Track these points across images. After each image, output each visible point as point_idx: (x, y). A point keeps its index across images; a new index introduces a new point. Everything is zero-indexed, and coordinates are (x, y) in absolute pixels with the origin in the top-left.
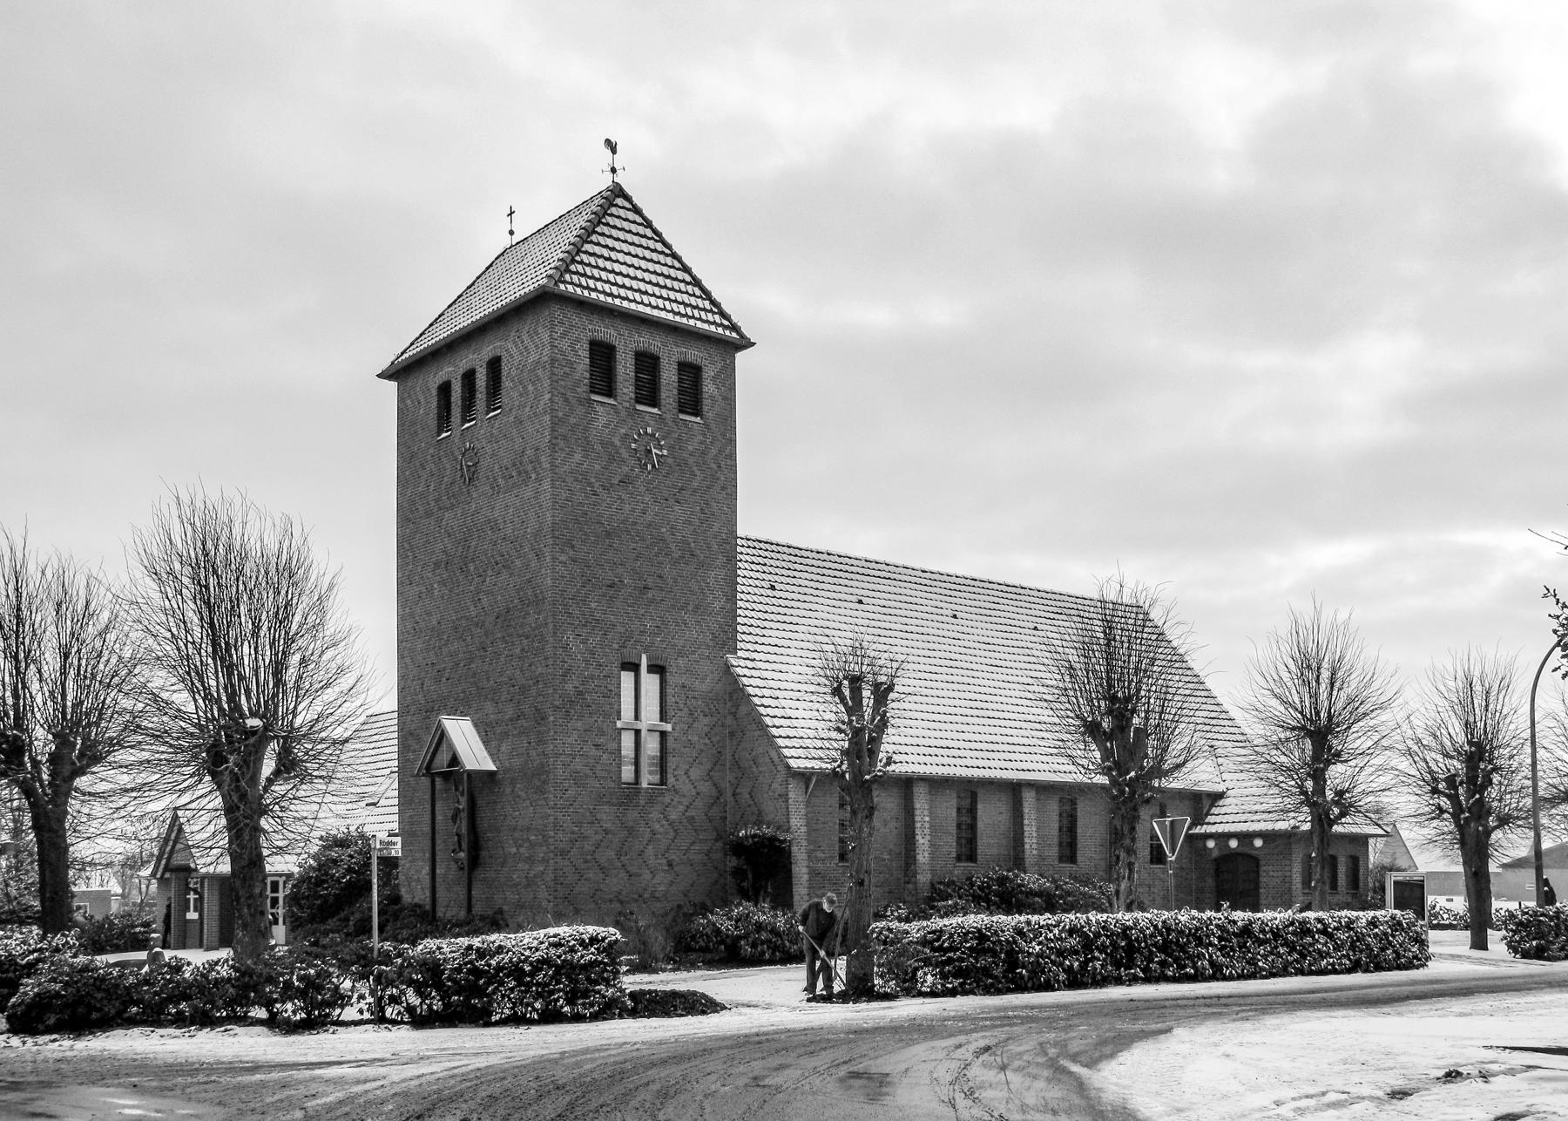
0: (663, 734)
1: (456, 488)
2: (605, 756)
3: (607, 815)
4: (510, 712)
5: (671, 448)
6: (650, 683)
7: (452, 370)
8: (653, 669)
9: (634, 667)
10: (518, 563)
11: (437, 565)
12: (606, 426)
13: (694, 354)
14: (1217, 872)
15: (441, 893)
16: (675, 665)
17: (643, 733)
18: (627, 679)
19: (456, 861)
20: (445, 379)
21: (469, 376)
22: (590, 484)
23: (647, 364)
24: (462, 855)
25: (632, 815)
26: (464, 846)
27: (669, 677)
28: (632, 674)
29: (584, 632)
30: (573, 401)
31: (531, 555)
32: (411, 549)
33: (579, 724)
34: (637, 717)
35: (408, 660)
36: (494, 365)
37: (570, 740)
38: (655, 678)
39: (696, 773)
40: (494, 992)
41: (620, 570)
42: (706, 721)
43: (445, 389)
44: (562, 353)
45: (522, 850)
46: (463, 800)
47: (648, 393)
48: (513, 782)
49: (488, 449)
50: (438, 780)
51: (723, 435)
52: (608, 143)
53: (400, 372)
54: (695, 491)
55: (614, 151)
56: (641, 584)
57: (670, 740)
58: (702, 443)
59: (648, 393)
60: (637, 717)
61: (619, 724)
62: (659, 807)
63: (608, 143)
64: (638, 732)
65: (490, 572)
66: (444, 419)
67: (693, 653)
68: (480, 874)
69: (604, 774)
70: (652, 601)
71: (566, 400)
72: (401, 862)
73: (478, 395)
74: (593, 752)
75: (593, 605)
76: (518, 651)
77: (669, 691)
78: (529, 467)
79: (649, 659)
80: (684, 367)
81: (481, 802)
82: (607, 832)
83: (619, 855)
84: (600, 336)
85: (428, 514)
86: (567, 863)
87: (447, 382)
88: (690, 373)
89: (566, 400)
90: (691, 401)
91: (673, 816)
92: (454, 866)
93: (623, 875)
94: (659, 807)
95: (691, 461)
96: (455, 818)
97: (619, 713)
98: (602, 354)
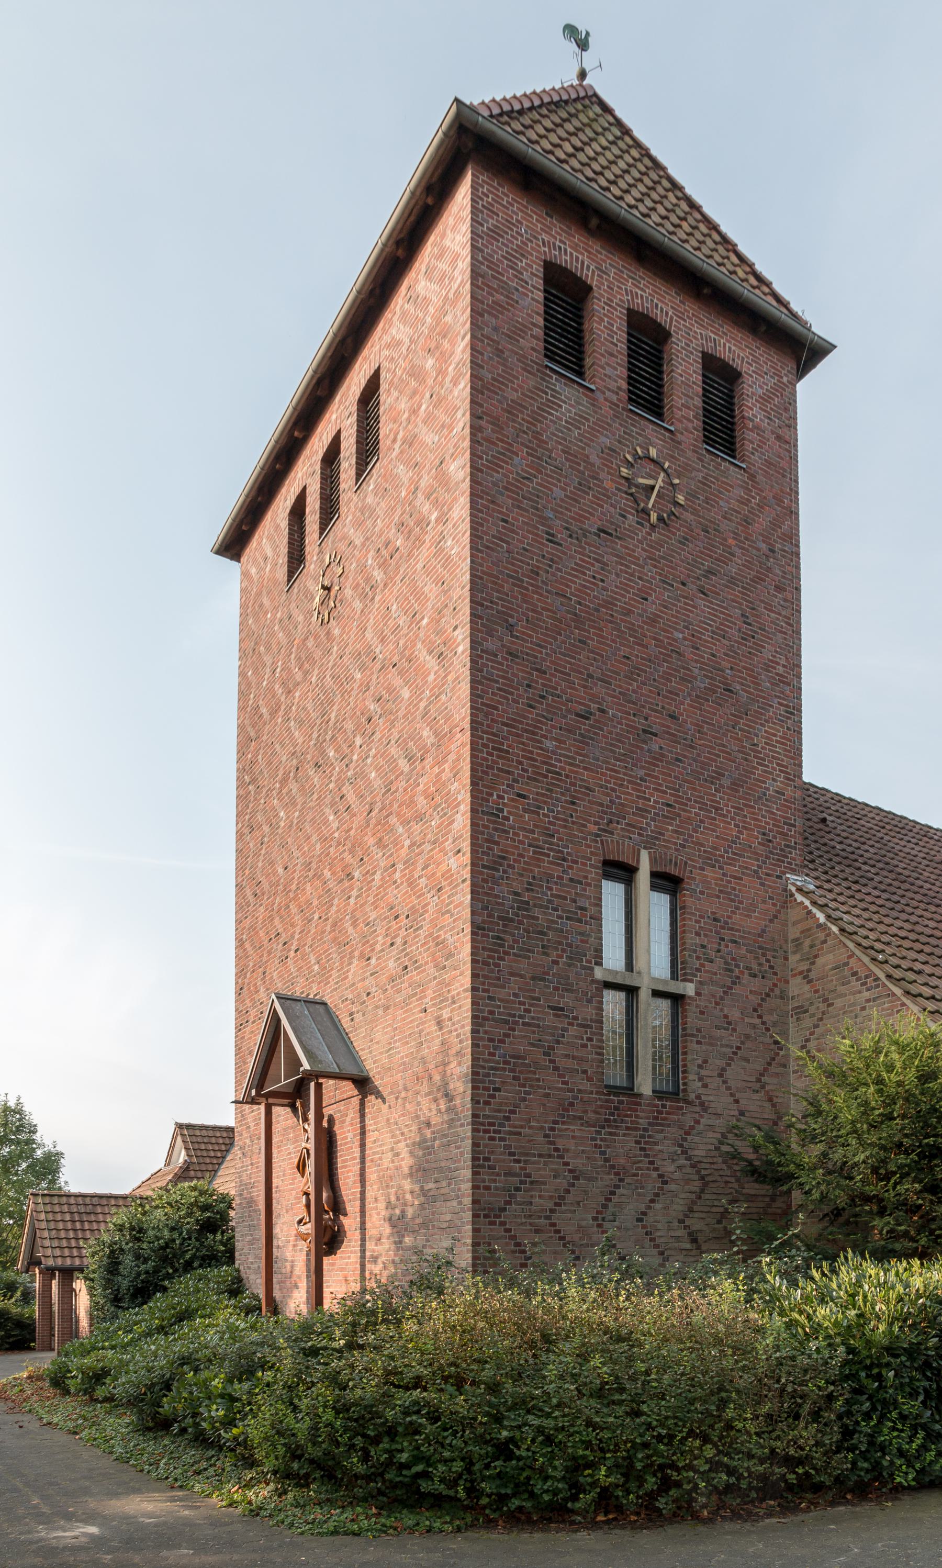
0: (677, 999)
2: (573, 1031)
3: (576, 1140)
6: (656, 909)
8: (666, 881)
9: (622, 871)
12: (574, 423)
13: (734, 347)
15: (352, 1114)
16: (702, 879)
17: (644, 995)
18: (612, 894)
22: (543, 520)
23: (647, 341)
25: (624, 1145)
27: (687, 897)
30: (512, 360)
33: (523, 966)
37: (502, 993)
39: (737, 1074)
41: (599, 689)
42: (756, 984)
47: (647, 391)
51: (779, 501)
52: (570, 30)
54: (732, 581)
55: (583, 45)
56: (640, 723)
57: (692, 1019)
58: (741, 502)
59: (647, 391)
61: (599, 974)
62: (674, 1132)
63: (570, 30)
64: (632, 991)
69: (571, 1064)
70: (658, 758)
71: (499, 352)
72: (594, 874)
74: (549, 1019)
75: (549, 744)
79: (653, 861)
82: (576, 1175)
83: (600, 1221)
84: (564, 260)
88: (720, 377)
89: (499, 352)
90: (721, 428)
91: (699, 1153)
94: (674, 1132)
95: (725, 526)
98: (566, 295)
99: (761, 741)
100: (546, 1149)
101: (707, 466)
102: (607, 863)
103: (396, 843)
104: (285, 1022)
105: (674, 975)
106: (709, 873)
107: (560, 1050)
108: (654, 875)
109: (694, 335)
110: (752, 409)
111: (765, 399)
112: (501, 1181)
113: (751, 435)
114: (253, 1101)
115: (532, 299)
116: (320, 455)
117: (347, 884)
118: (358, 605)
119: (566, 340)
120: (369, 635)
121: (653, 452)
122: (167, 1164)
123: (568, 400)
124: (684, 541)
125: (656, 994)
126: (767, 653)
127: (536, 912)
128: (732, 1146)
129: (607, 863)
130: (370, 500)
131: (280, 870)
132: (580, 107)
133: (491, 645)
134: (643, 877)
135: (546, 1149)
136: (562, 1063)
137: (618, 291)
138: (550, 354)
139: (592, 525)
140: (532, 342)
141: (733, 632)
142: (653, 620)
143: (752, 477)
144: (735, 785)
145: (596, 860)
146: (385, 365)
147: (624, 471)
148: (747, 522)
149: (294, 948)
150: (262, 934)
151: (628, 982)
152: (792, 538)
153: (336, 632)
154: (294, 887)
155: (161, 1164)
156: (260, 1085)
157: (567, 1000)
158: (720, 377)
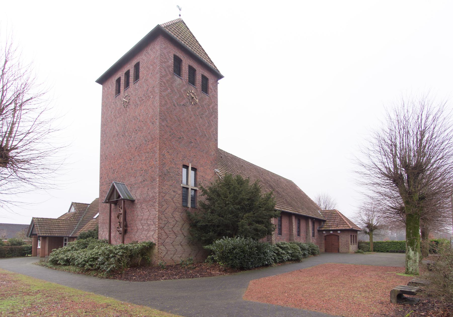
0: (195, 190)
1: (122, 110)
4: (140, 179)
6: (192, 173)
7: (121, 74)
8: (193, 169)
9: (186, 167)
10: (145, 128)
11: (114, 136)
12: (179, 85)
13: (207, 74)
14: (325, 239)
16: (200, 169)
17: (190, 189)
18: (184, 170)
19: (119, 231)
20: (118, 77)
21: (127, 74)
22: (173, 102)
23: (192, 71)
24: (121, 229)
26: (122, 225)
28: (186, 170)
29: (170, 151)
31: (150, 124)
32: (105, 134)
34: (187, 184)
35: (103, 168)
36: (137, 66)
37: (164, 188)
38: (193, 172)
40: (133, 276)
43: (119, 81)
44: (164, 54)
45: (145, 227)
46: (122, 211)
47: (192, 81)
48: (141, 204)
49: (134, 94)
50: (113, 205)
51: (215, 102)
52: (178, 7)
53: (102, 80)
55: (180, 10)
59: (192, 81)
60: (187, 184)
61: (182, 185)
63: (178, 7)
65: (133, 134)
66: (118, 91)
67: (205, 166)
68: (127, 236)
72: (181, 167)
73: (131, 77)
74: (173, 193)
75: (174, 143)
76: (144, 158)
77: (198, 177)
78: (150, 94)
79: (192, 165)
80: (203, 77)
81: (128, 211)
82: (177, 221)
85: (112, 121)
86: (163, 231)
87: (119, 77)
88: (205, 79)
90: (205, 88)
92: (118, 233)
93: (172, 242)
96: (118, 217)
97: (182, 181)
98: (178, 61)
99: (211, 145)
100: (172, 217)
101: (203, 95)
102: (183, 165)
103: (142, 156)
104: (116, 187)
105: (195, 186)
106: (201, 168)
107: (175, 199)
108: (192, 168)
109: (200, 72)
110: (210, 86)
111: (212, 84)
112: (163, 222)
113: (210, 90)
114: (107, 203)
115: (171, 62)
117: (130, 161)
118: (133, 107)
119: (178, 70)
120: (136, 114)
122: (69, 211)
123: (178, 80)
124: (198, 108)
125: (192, 189)
126: (212, 129)
127: (171, 173)
129: (183, 165)
130: (137, 87)
131: (113, 155)
132: (180, 25)
134: (190, 168)
135: (172, 217)
136: (175, 201)
137: (186, 62)
138: (174, 71)
139: (182, 103)
140: (171, 69)
141: (206, 125)
142: (192, 122)
143: (210, 98)
144: (206, 153)
145: (182, 165)
146: (141, 62)
147: (188, 94)
148: (209, 106)
149: (117, 171)
150: (107, 167)
151: (187, 187)
152: (217, 109)
153: (128, 110)
154: (116, 159)
155: (67, 211)
156: (109, 199)
157: (176, 190)
158: (205, 79)
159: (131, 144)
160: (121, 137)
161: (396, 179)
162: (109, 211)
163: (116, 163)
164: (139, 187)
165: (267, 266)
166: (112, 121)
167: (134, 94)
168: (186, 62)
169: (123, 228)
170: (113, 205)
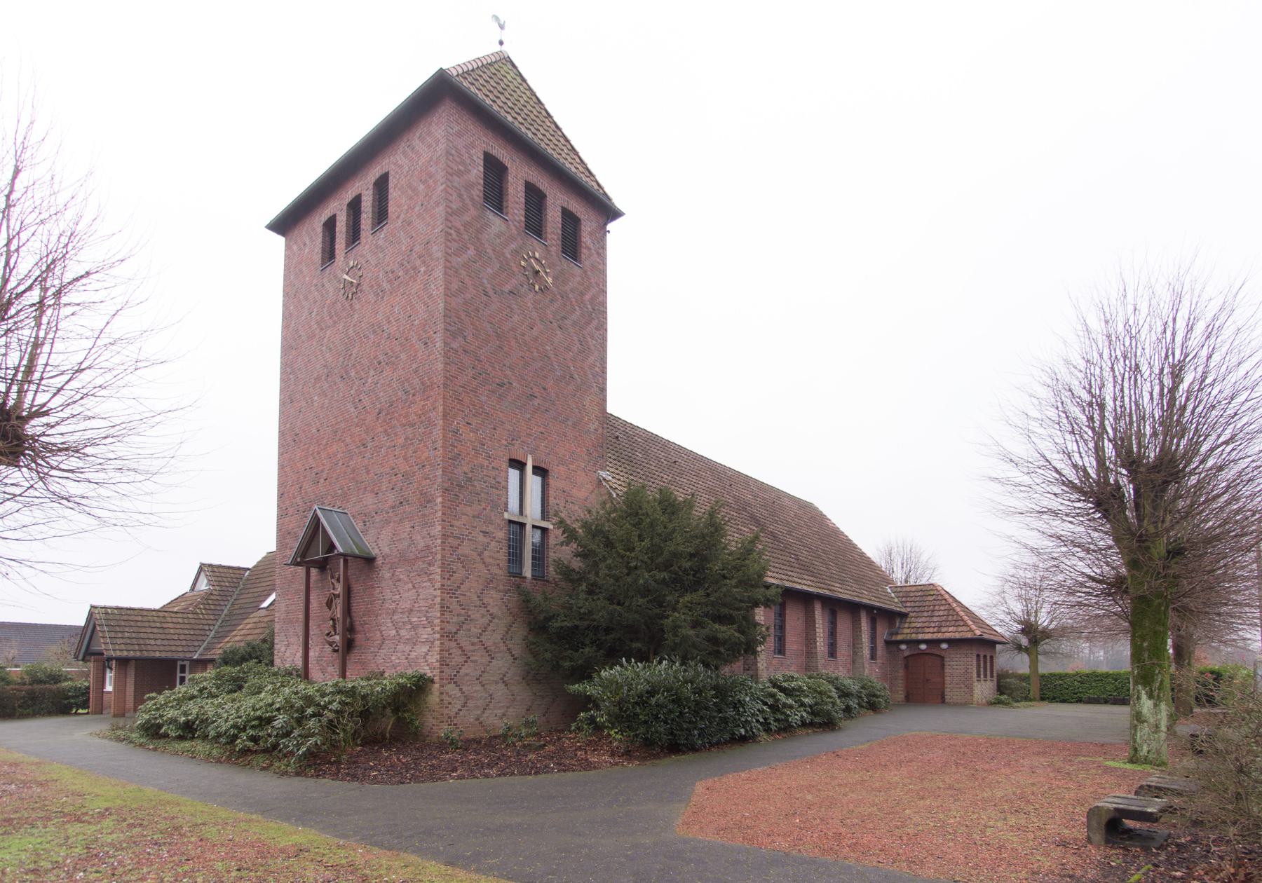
0: (544, 531)
1: (339, 306)
4: (391, 498)
5: (555, 278)
6: (534, 482)
7: (337, 207)
8: (538, 470)
9: (519, 465)
10: (403, 356)
11: (318, 379)
12: (498, 236)
13: (576, 207)
14: (906, 667)
16: (556, 472)
17: (529, 528)
18: (514, 474)
19: (331, 644)
20: (330, 215)
22: (482, 284)
23: (535, 198)
24: (337, 638)
26: (339, 628)
28: (517, 472)
29: (474, 421)
31: (419, 345)
32: (293, 372)
34: (521, 512)
35: (287, 469)
36: (382, 185)
37: (457, 523)
38: (538, 479)
43: (330, 225)
44: (457, 150)
45: (403, 632)
46: (339, 589)
47: (534, 225)
48: (393, 567)
49: (373, 261)
50: (314, 571)
51: (598, 285)
52: (496, 18)
53: (285, 224)
55: (502, 27)
59: (534, 225)
60: (521, 512)
61: (506, 516)
63: (496, 18)
65: (372, 373)
66: (329, 254)
67: (572, 463)
68: (353, 657)
72: (505, 465)
73: (364, 216)
74: (481, 538)
75: (483, 398)
76: (401, 441)
77: (552, 492)
78: (418, 262)
79: (534, 460)
80: (566, 213)
81: (357, 588)
82: (493, 616)
85: (311, 337)
86: (453, 644)
87: (332, 213)
88: (571, 221)
90: (571, 246)
92: (328, 649)
93: (479, 673)
96: (329, 604)
97: (506, 504)
98: (495, 171)
99: (587, 403)
100: (478, 603)
101: (566, 264)
102: (511, 460)
104: (323, 520)
105: (543, 518)
106: (561, 467)
107: (486, 554)
108: (534, 467)
109: (557, 200)
110: (586, 239)
111: (591, 234)
112: (455, 619)
113: (584, 251)
114: (298, 564)
115: (477, 172)
116: (347, 201)
117: (362, 449)
118: (372, 297)
119: (495, 195)
120: (380, 316)
121: (537, 255)
122: (193, 589)
123: (496, 223)
124: (552, 301)
125: (534, 527)
126: (591, 360)
127: (476, 483)
128: (12, 317)
129: (511, 460)
131: (314, 431)
132: (500, 68)
133: (455, 345)
134: (529, 468)
135: (478, 603)
136: (487, 560)
137: (519, 174)
138: (486, 198)
139: (507, 288)
140: (478, 192)
142: (536, 339)
143: (585, 272)
144: (575, 425)
145: (506, 459)
146: (392, 173)
148: (582, 294)
149: (325, 476)
151: (521, 520)
152: (604, 304)
154: (324, 442)
155: (187, 589)
156: (304, 555)
157: (490, 529)
158: (571, 221)
159: (366, 401)
160: (338, 380)
161: (1103, 499)
162: (303, 587)
163: (323, 455)
164: (387, 522)
165: (743, 740)
166: (311, 337)
167: (373, 261)
168: (519, 174)
169: (344, 636)
170: (314, 571)
